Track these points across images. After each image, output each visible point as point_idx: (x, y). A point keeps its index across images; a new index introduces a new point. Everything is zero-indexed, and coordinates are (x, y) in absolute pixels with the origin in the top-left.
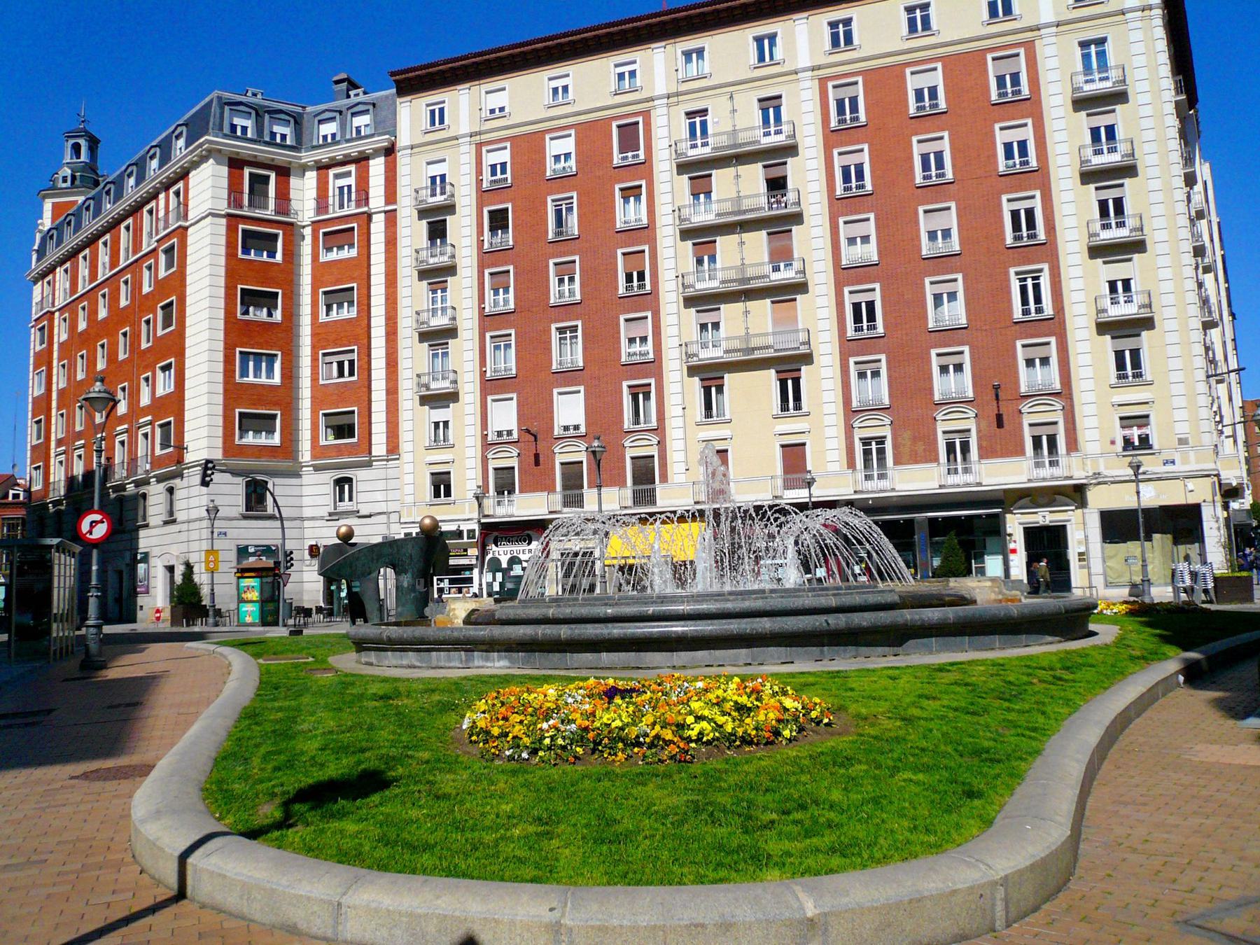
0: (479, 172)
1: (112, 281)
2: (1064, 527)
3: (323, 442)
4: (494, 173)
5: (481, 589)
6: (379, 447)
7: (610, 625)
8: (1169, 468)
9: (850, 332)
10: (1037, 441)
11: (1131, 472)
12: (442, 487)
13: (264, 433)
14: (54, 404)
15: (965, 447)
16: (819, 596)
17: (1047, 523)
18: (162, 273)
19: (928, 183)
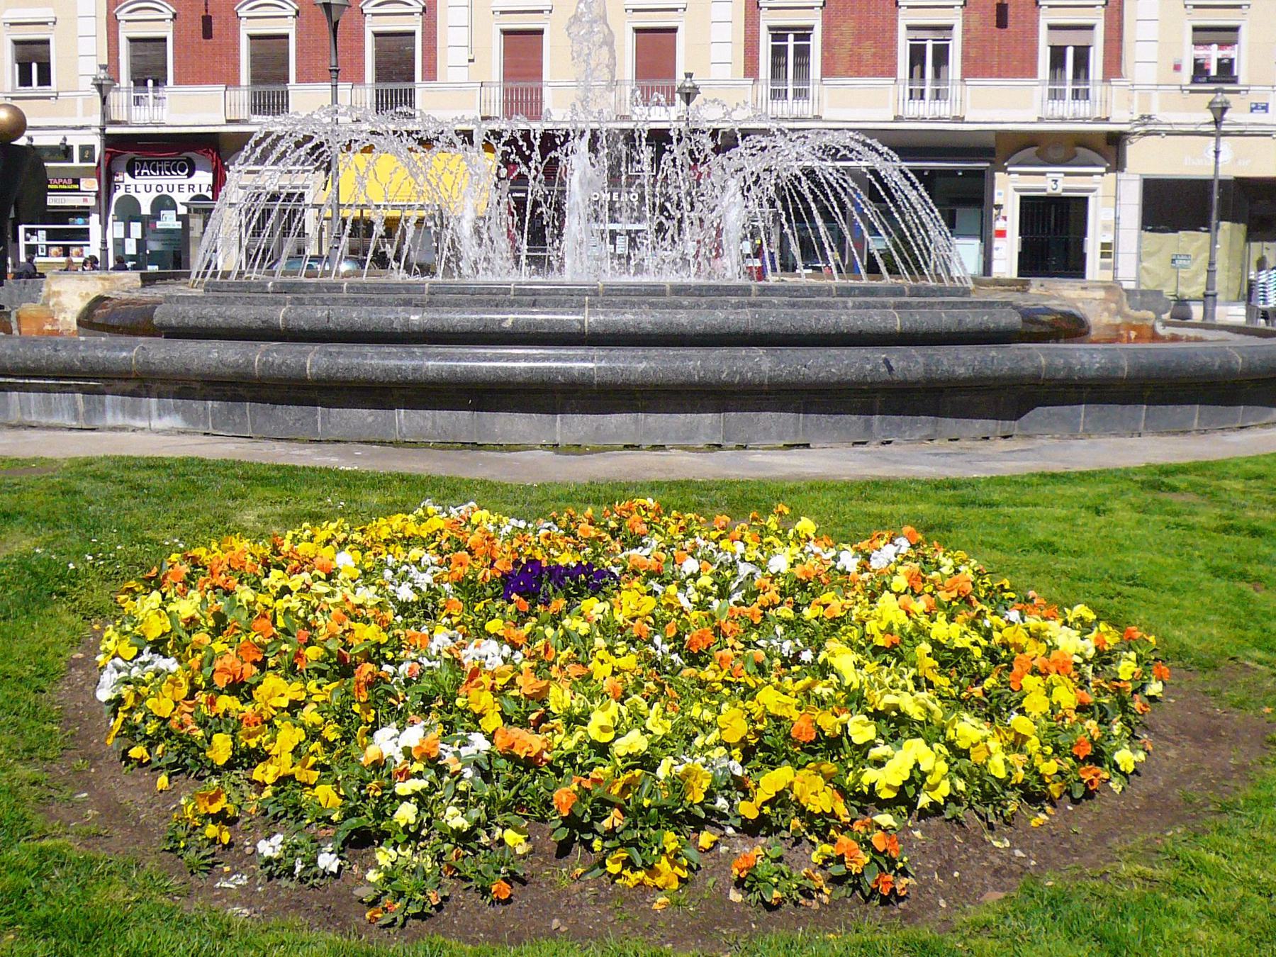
2: (1085, 200)
5: (104, 251)
7: (417, 350)
8: (1259, 117)
10: (1058, 55)
11: (1210, 117)
12: (34, 66)
15: (941, 55)
16: (868, 306)
17: (1059, 191)
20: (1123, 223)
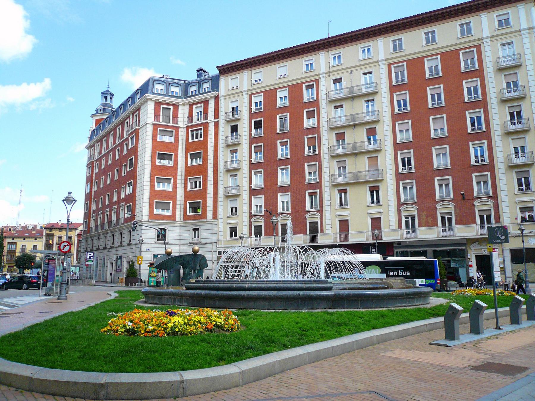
0: (251, 105)
1: (113, 150)
3: (188, 213)
4: (256, 106)
6: (210, 215)
9: (400, 170)
12: (234, 233)
13: (165, 210)
14: (93, 197)
15: (450, 220)
18: (130, 147)
19: (434, 106)
20: (506, 262)
